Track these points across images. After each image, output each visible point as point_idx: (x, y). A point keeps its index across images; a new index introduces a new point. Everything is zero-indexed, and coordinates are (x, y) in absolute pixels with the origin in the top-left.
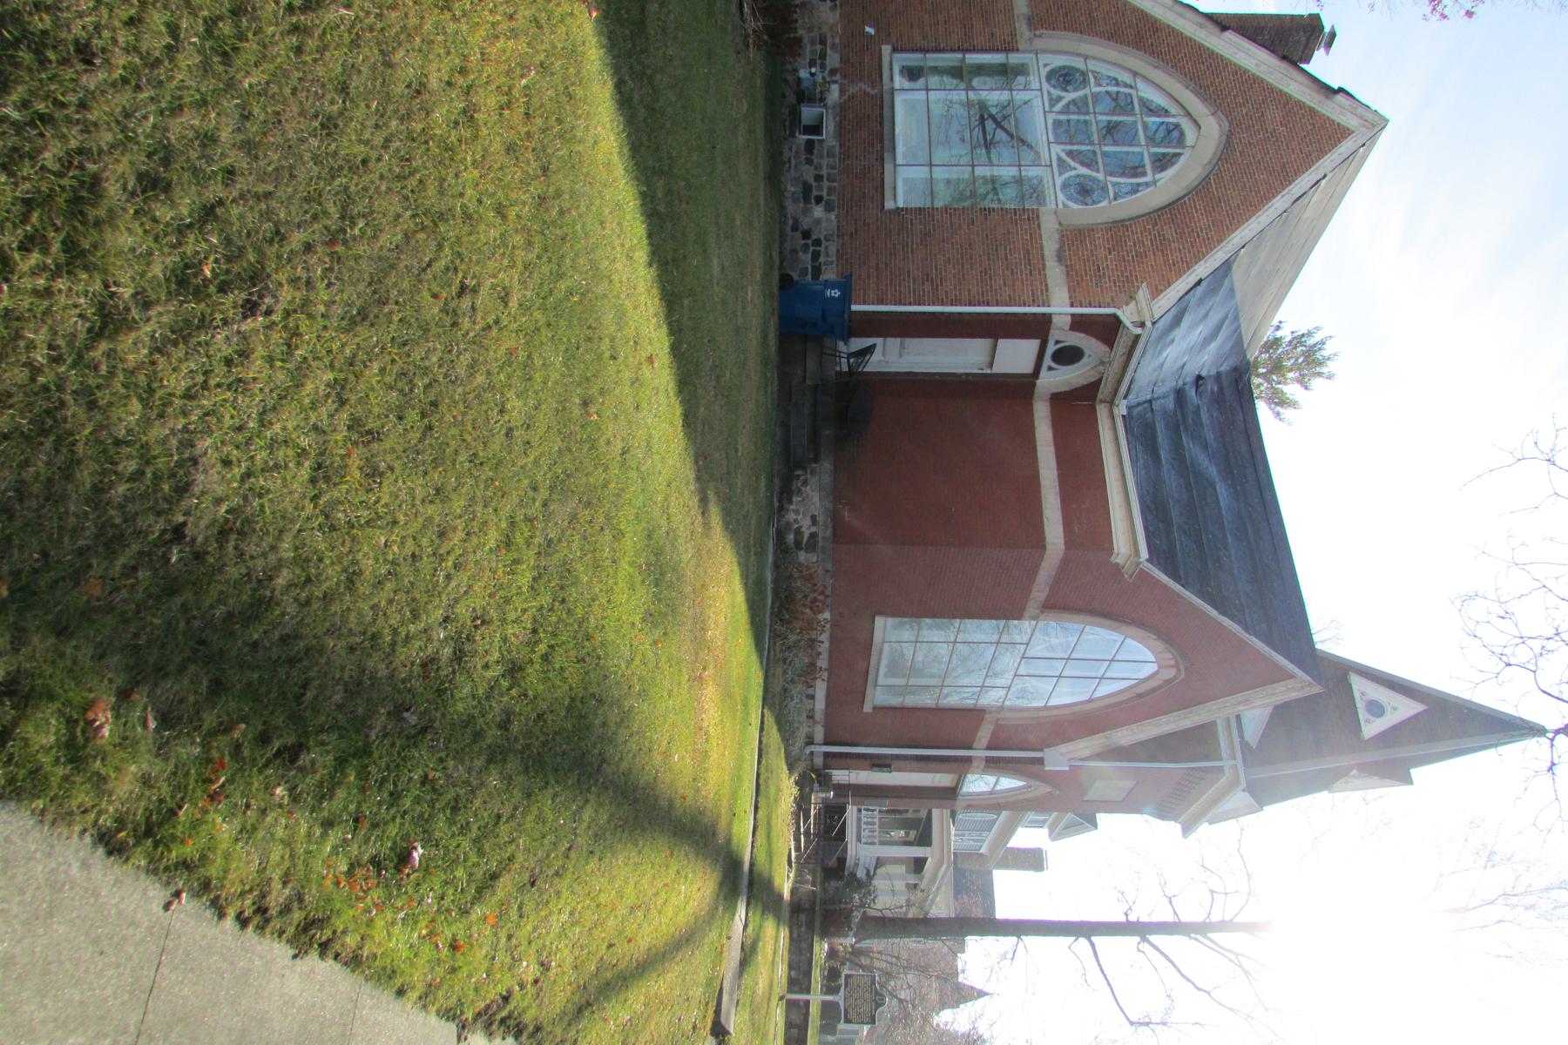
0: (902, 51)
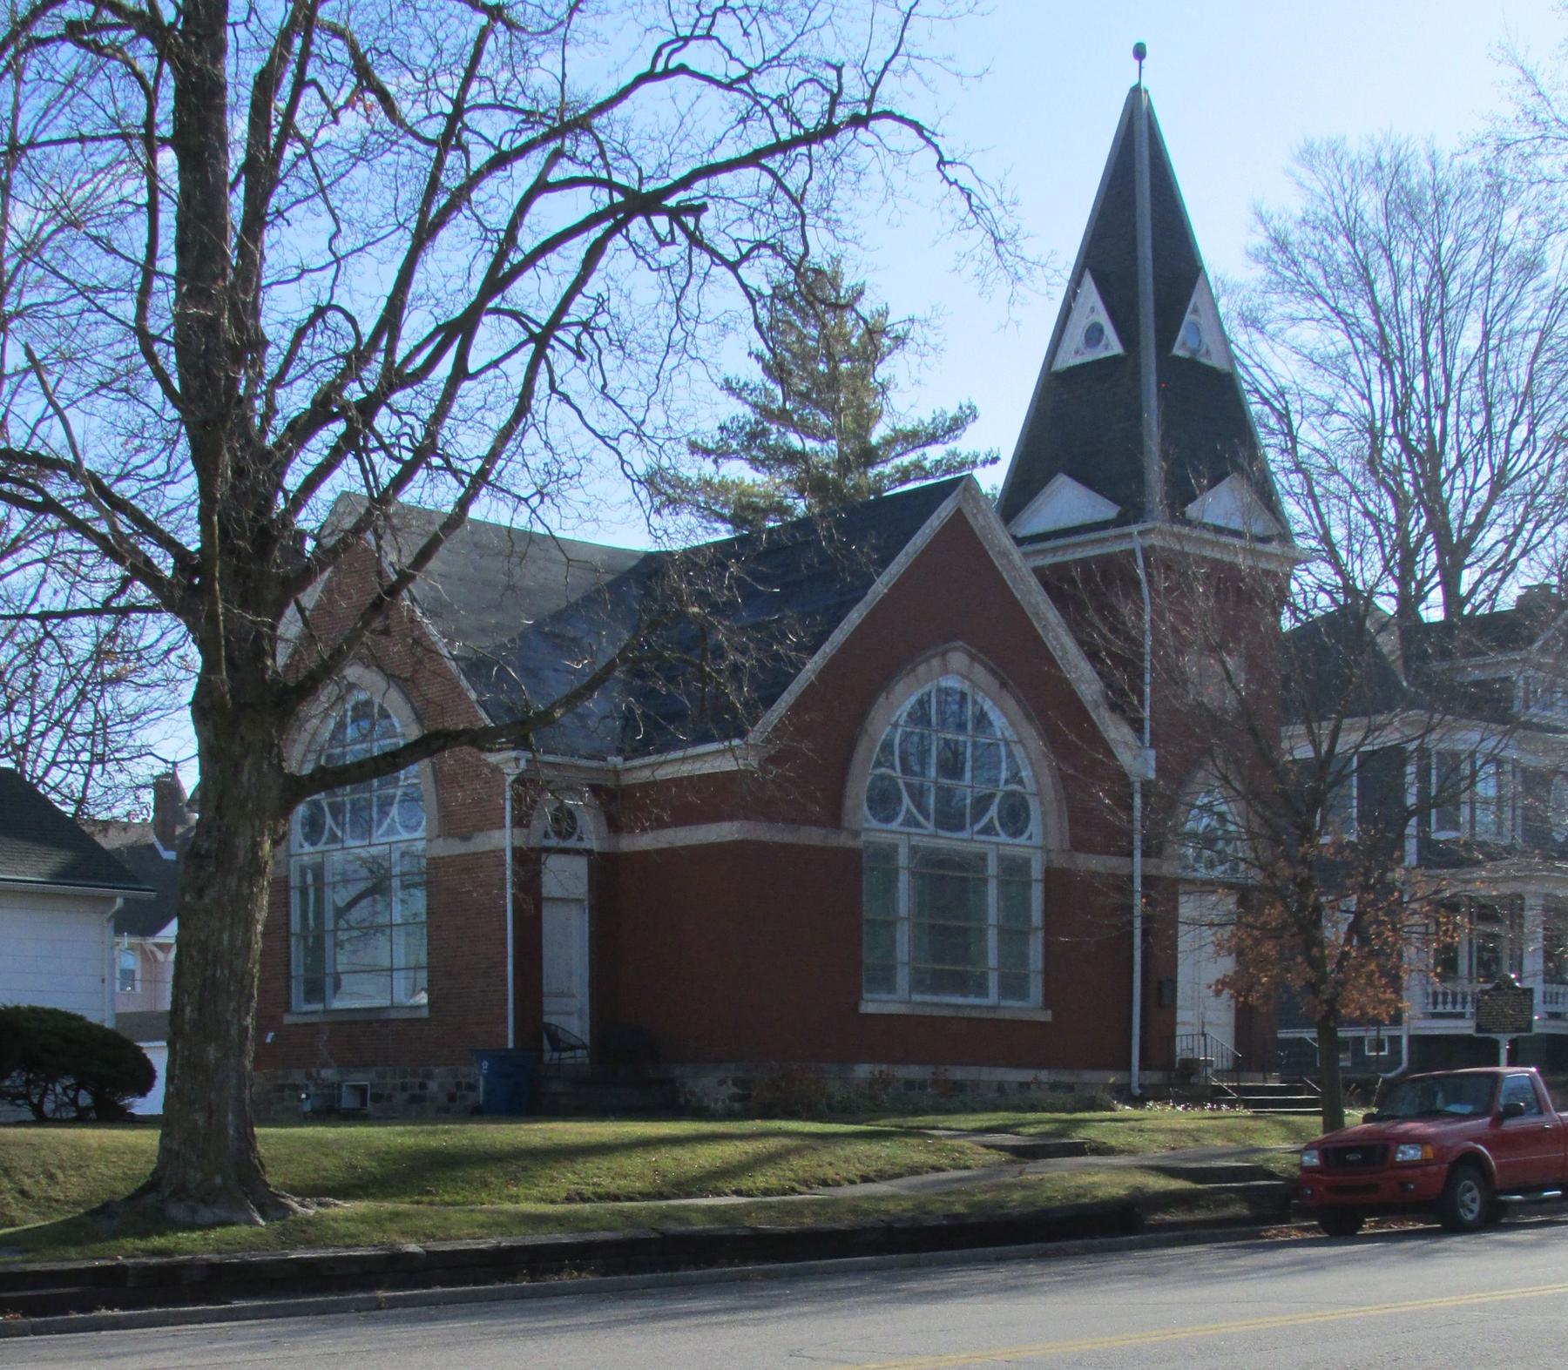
0: (288, 1002)
